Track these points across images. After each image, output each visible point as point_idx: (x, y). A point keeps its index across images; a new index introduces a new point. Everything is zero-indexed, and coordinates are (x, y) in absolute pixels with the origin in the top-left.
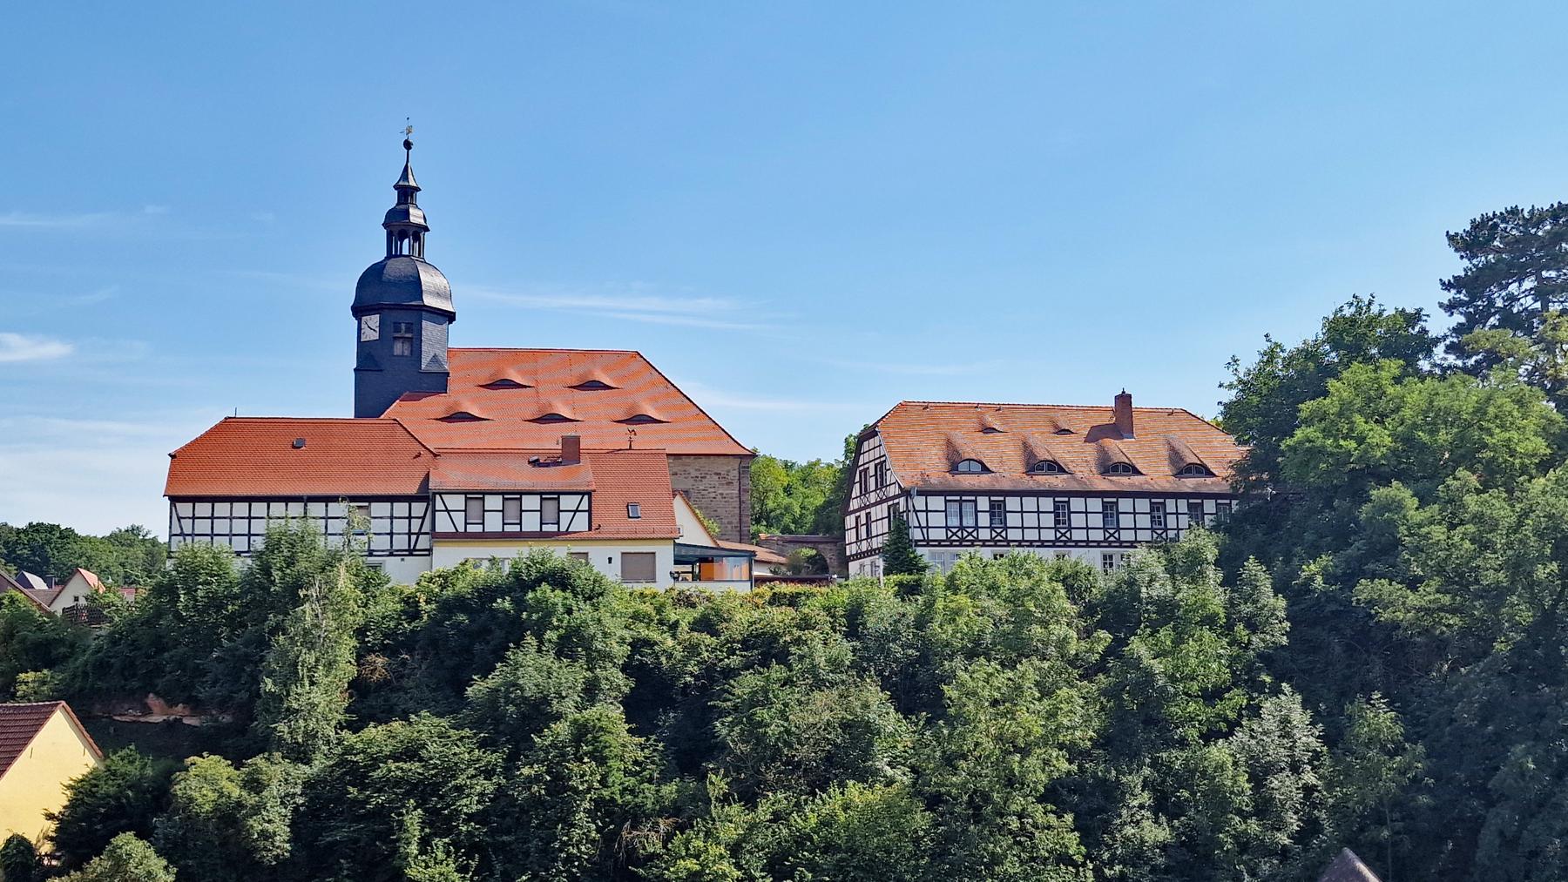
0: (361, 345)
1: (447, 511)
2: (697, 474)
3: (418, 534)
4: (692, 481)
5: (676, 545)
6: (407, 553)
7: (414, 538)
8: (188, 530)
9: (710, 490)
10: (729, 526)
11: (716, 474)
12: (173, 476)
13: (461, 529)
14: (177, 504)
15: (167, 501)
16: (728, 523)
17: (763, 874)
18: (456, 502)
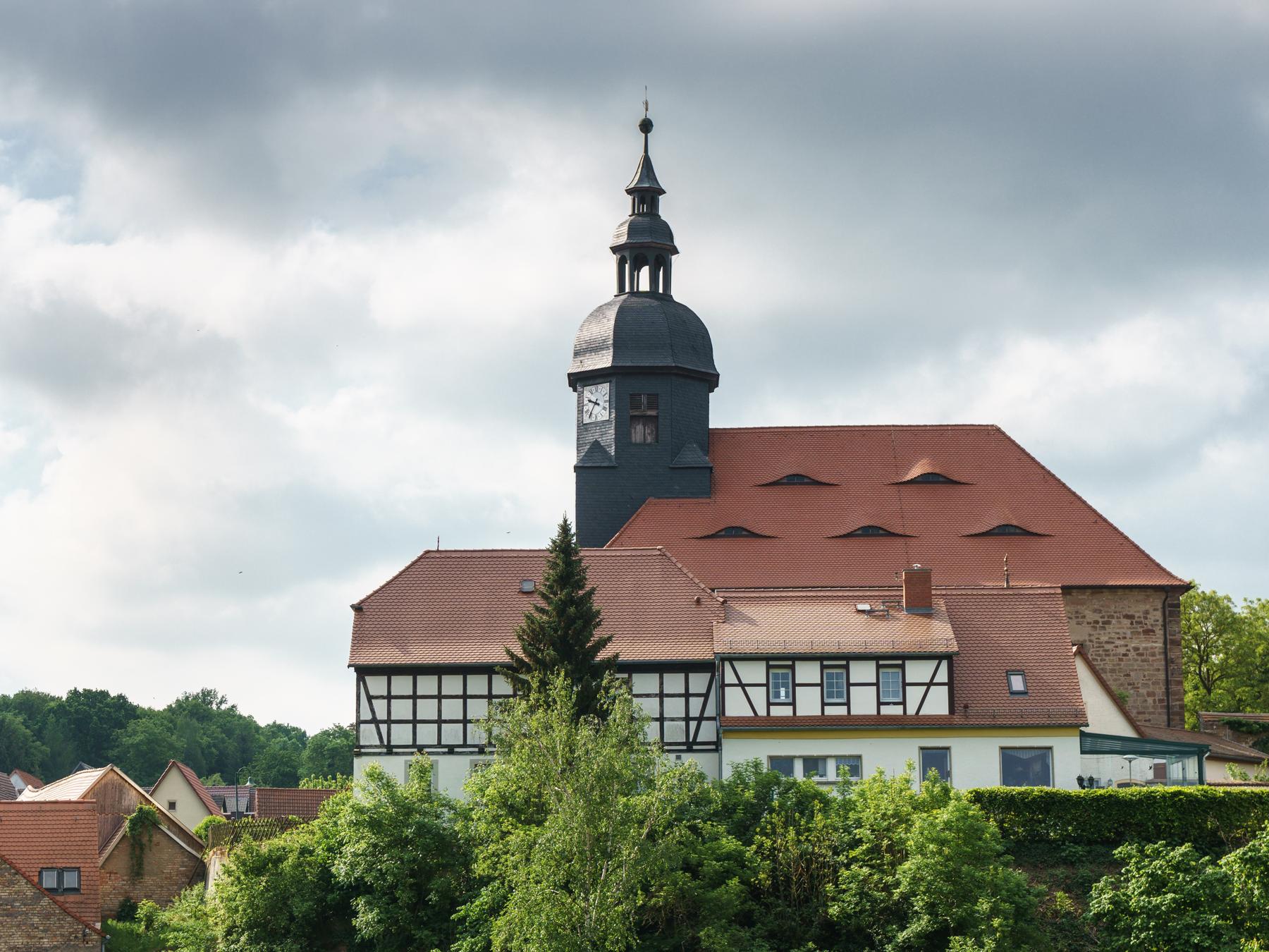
0: (582, 428)
1: (742, 685)
2: (1097, 617)
3: (700, 719)
4: (1088, 629)
5: (1083, 735)
6: (685, 748)
7: (693, 725)
8: (381, 714)
9: (1118, 642)
10: (1150, 700)
11: (1127, 617)
12: (360, 638)
13: (762, 712)
14: (367, 678)
15: (352, 674)
16: (1149, 694)
18: (754, 673)
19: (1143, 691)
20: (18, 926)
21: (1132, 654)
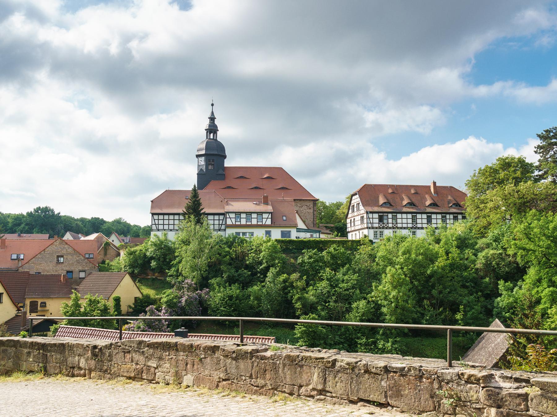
10: (310, 222)
11: (306, 205)
19: (309, 220)
21: (307, 213)
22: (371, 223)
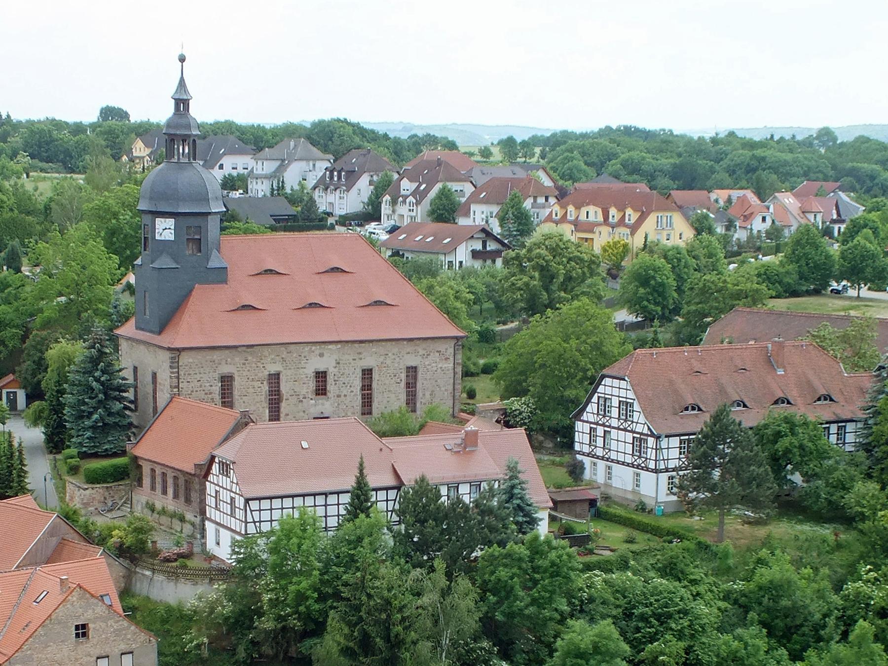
7: (390, 513)
8: (257, 519)
10: (446, 393)
11: (437, 352)
17: (68, 374)
19: (443, 389)
20: (122, 640)
21: (439, 370)
22: (664, 460)
